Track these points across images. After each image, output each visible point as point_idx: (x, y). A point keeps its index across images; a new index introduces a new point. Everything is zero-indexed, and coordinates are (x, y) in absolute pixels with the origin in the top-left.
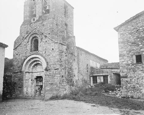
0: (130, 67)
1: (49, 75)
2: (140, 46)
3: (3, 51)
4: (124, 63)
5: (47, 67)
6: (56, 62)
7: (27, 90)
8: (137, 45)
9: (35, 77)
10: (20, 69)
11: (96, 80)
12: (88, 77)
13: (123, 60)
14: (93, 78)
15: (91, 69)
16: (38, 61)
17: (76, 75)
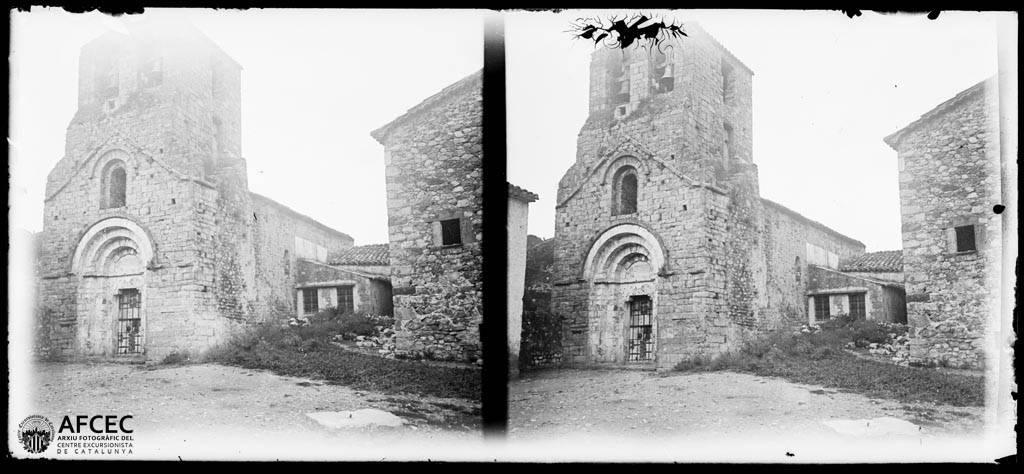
2: (970, 196)
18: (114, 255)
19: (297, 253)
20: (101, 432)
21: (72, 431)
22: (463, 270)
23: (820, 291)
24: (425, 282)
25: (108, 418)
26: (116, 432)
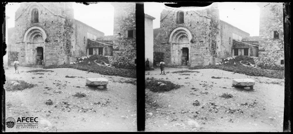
0: (122, 41)
1: (194, 46)
2: (279, 22)
4: (263, 38)
5: (192, 39)
6: (56, 34)
7: (174, 60)
8: (276, 21)
9: (182, 48)
10: (21, 39)
11: (238, 52)
12: (230, 49)
13: (263, 35)
14: (89, 50)
15: (88, 41)
16: (184, 33)
17: (74, 46)
19: (88, 38)
20: (29, 122)
21: (21, 122)
22: (133, 44)
24: (122, 47)
25: (31, 118)
26: (33, 122)
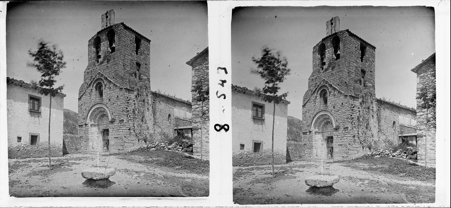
3: (61, 101)
18: (101, 117)
23: (180, 128)
